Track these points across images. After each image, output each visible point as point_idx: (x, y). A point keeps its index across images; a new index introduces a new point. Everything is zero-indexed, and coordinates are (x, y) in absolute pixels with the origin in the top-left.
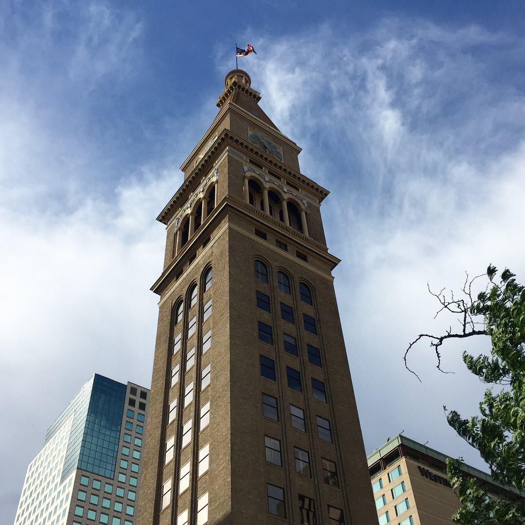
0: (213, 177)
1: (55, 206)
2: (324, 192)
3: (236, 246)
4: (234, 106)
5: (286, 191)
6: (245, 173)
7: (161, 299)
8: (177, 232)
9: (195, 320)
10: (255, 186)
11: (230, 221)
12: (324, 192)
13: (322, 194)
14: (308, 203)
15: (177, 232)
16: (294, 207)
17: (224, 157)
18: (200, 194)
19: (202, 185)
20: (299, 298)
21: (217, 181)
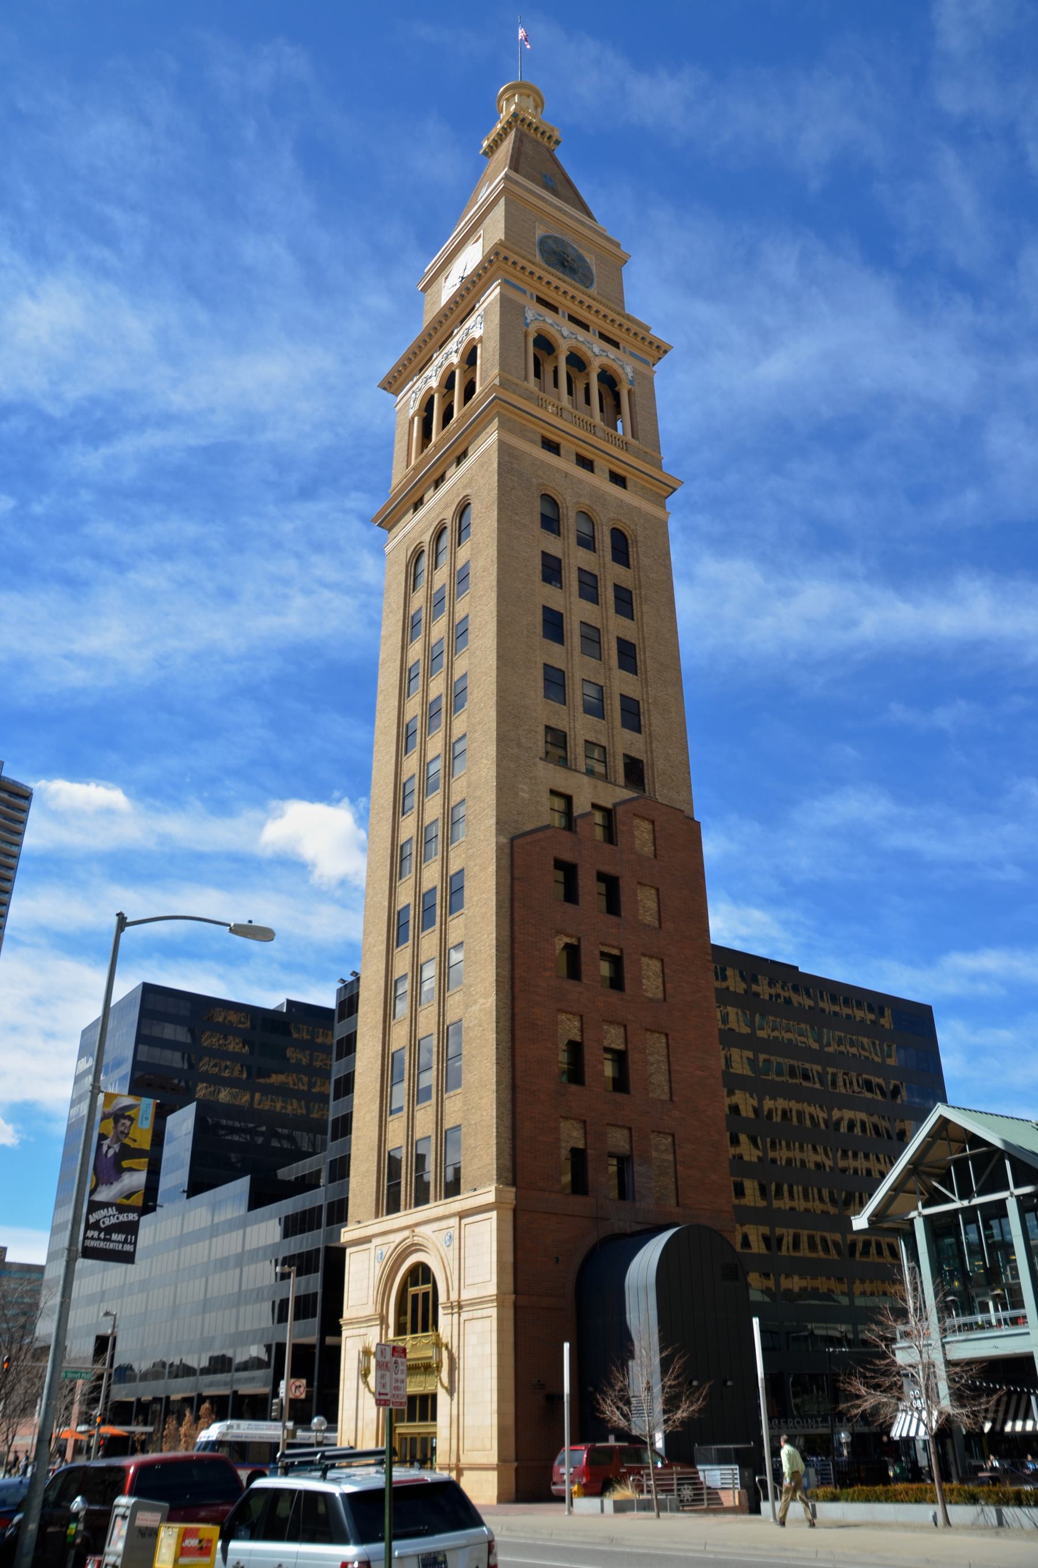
0: (475, 327)
1: (3, 1117)
2: (663, 348)
3: (508, 459)
4: (516, 183)
5: (597, 352)
6: (527, 325)
7: (362, 819)
8: (413, 418)
9: (426, 987)
10: (544, 345)
11: (501, 427)
12: (663, 348)
13: (661, 350)
14: (635, 371)
15: (413, 418)
16: (609, 380)
17: (493, 293)
18: (451, 354)
19: (456, 340)
20: (612, 610)
21: (481, 339)
